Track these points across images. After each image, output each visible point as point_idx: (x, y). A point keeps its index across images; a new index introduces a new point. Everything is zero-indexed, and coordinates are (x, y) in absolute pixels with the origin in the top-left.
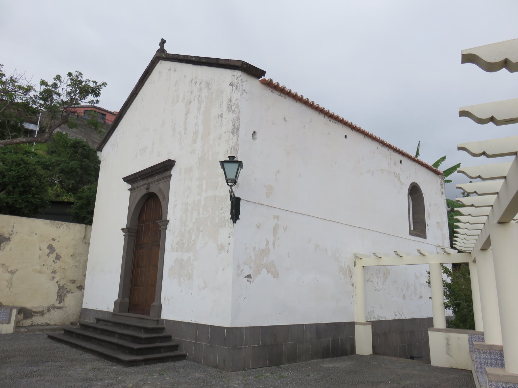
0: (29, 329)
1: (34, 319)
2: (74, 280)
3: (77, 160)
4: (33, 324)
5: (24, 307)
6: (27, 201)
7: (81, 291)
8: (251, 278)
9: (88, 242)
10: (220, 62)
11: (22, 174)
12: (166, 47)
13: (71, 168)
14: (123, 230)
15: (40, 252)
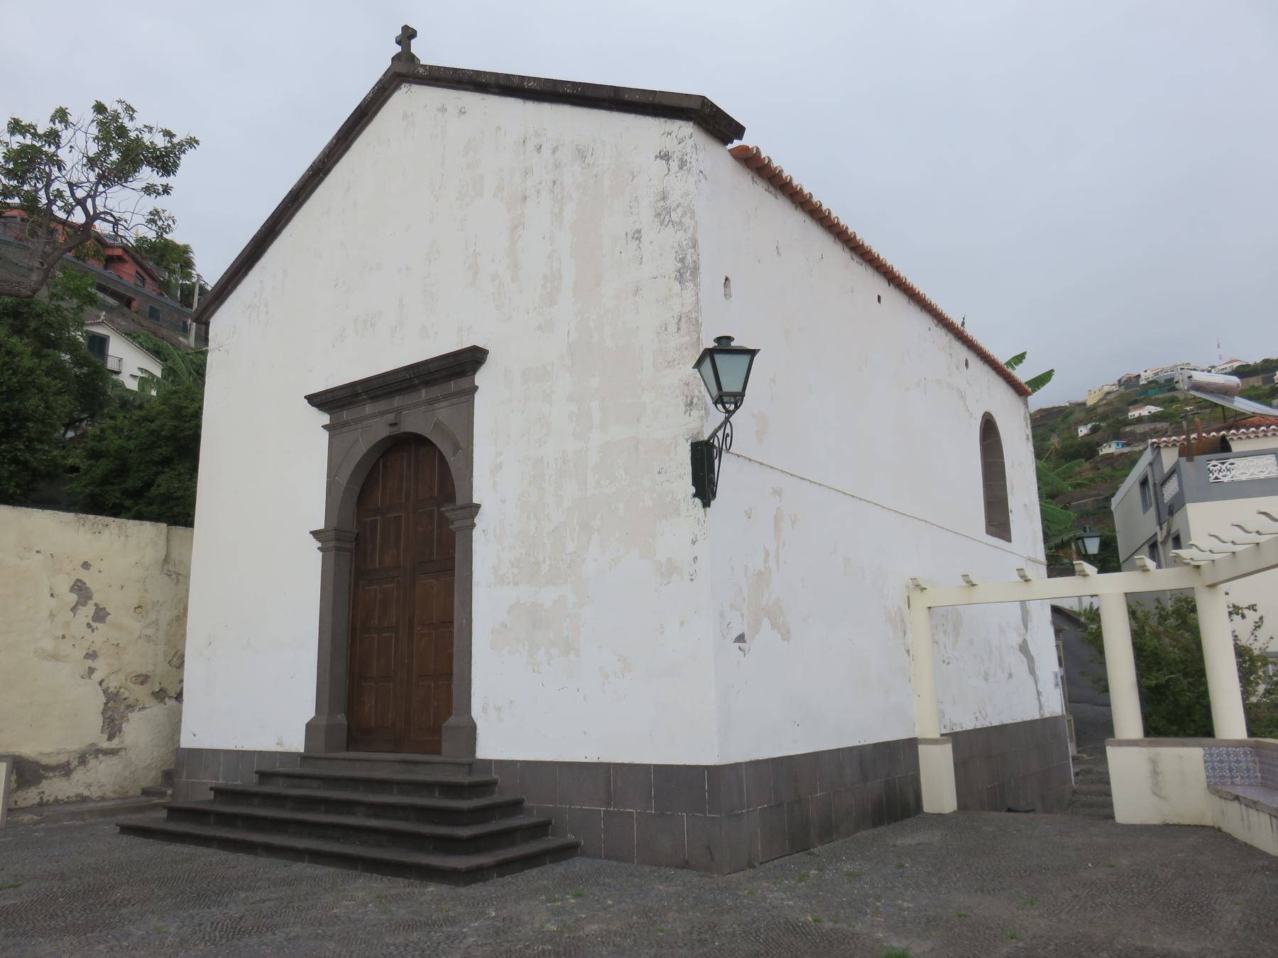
0: (41, 815)
2: (145, 673)
4: (44, 800)
6: (15, 460)
7: (162, 705)
8: (745, 642)
9: (175, 572)
10: (626, 96)
12: (416, 47)
14: (316, 534)
15: (53, 601)
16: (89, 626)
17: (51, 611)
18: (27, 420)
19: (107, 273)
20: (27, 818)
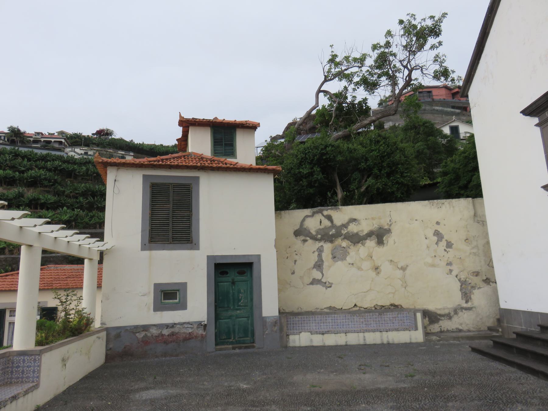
1: (441, 322)
3: (421, 141)
5: (426, 309)
6: (397, 183)
7: (490, 286)
9: (481, 221)
11: (384, 152)
13: (418, 151)
15: (427, 241)
16: (445, 250)
17: (427, 245)
18: (398, 164)
19: (454, 100)
20: (434, 338)
